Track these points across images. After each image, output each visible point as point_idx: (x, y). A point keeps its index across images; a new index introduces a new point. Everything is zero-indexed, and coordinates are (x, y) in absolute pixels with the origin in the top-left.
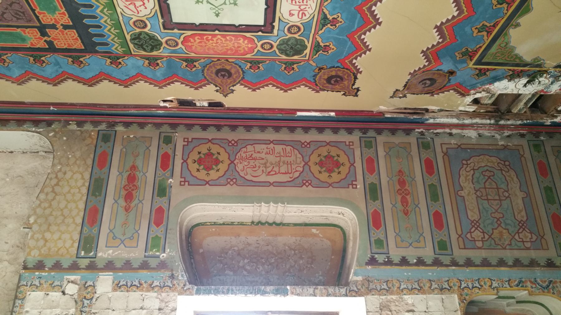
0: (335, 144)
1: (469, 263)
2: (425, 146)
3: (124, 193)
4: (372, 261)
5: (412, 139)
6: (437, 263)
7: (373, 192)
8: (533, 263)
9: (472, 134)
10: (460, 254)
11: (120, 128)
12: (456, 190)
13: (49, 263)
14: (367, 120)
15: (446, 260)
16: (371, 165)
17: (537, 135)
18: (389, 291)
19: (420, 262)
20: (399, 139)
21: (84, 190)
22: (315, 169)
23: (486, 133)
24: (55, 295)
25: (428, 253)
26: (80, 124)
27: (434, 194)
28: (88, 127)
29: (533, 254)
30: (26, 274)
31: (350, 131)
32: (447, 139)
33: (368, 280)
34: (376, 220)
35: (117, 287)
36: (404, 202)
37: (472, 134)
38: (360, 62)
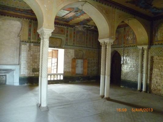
0: (63, 28)
1: (76, 46)
2: (74, 30)
3: (34, 32)
4: (66, 45)
5: (73, 29)
6: (73, 46)
7: (67, 36)
8: (83, 47)
9: (80, 29)
10: (75, 45)
11: (32, 21)
12: (77, 37)
13: (24, 41)
14: (104, 66)
15: (74, 45)
16: (67, 32)
17: (88, 30)
18: (67, 49)
19: (71, 46)
20: (71, 28)
21: (28, 31)
22: (60, 31)
23: (82, 29)
24: (25, 46)
25: (72, 44)
26: (26, 19)
27: (74, 37)
28: (27, 20)
29: (83, 46)
30: (21, 42)
31: (65, 26)
32: (77, 29)
33: (65, 47)
34: (67, 40)
35: (34, 45)
36: (71, 37)
37: (80, 29)
38: (70, 21)
